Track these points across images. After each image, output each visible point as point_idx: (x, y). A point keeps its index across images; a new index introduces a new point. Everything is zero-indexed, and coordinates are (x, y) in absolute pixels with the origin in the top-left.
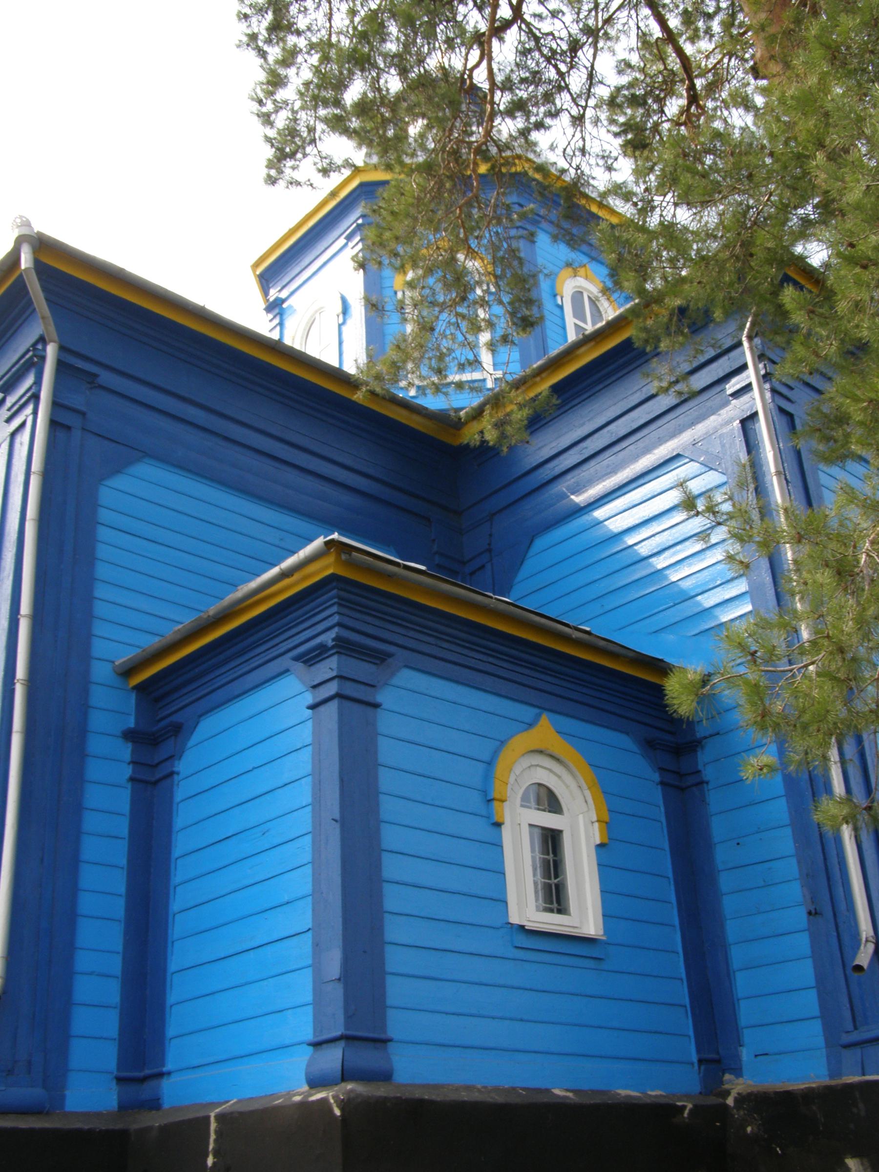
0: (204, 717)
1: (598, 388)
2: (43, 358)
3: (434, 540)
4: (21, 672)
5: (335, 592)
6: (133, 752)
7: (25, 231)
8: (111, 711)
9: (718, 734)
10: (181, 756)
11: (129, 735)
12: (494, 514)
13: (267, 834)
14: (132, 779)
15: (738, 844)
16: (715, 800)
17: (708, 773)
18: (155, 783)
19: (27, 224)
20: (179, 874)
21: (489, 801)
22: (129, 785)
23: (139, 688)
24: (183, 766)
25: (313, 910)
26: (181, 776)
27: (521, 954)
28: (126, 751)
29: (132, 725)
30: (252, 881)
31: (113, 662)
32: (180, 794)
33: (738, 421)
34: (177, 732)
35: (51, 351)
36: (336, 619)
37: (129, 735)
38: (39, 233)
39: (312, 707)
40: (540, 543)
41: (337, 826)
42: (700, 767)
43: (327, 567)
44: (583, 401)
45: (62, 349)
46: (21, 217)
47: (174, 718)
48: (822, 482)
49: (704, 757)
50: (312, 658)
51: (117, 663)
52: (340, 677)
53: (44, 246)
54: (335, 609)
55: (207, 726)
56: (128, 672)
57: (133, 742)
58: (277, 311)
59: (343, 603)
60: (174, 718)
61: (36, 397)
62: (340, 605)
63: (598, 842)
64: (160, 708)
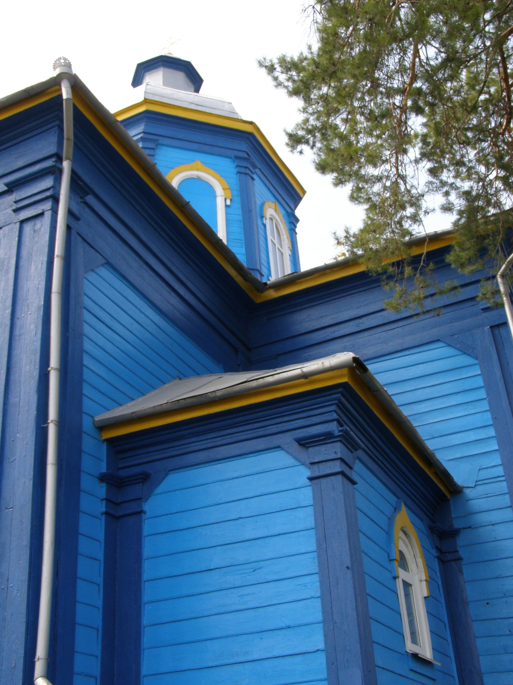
0: (171, 472)
1: (373, 286)
2: (60, 171)
3: (239, 365)
5: (339, 395)
6: (107, 490)
8: (95, 460)
9: (470, 527)
10: (147, 500)
11: (102, 478)
12: (279, 355)
13: (257, 571)
14: (106, 513)
15: (488, 604)
16: (468, 572)
17: (462, 553)
18: (118, 518)
19: (69, 65)
20: (148, 592)
21: (391, 560)
22: (103, 518)
23: (110, 441)
24: (148, 507)
25: (325, 636)
26: (147, 515)
27: (412, 675)
28: (102, 490)
29: (104, 470)
30: (244, 607)
31: (93, 417)
32: (147, 528)
33: (489, 327)
34: (146, 480)
35: (66, 165)
36: (335, 416)
37: (102, 478)
38: (75, 75)
39: (311, 479)
41: (349, 575)
42: (458, 549)
43: (342, 376)
44: (360, 292)
46: (65, 59)
47: (146, 468)
48: (85, 362)
49: (461, 540)
50: (304, 443)
51: (97, 419)
52: (342, 460)
53: (78, 88)
54: (334, 408)
55: (174, 480)
56: (102, 427)
57: (107, 483)
59: (340, 405)
60: (146, 468)
61: (56, 199)
62: (338, 406)
63: (426, 594)
64: (121, 459)
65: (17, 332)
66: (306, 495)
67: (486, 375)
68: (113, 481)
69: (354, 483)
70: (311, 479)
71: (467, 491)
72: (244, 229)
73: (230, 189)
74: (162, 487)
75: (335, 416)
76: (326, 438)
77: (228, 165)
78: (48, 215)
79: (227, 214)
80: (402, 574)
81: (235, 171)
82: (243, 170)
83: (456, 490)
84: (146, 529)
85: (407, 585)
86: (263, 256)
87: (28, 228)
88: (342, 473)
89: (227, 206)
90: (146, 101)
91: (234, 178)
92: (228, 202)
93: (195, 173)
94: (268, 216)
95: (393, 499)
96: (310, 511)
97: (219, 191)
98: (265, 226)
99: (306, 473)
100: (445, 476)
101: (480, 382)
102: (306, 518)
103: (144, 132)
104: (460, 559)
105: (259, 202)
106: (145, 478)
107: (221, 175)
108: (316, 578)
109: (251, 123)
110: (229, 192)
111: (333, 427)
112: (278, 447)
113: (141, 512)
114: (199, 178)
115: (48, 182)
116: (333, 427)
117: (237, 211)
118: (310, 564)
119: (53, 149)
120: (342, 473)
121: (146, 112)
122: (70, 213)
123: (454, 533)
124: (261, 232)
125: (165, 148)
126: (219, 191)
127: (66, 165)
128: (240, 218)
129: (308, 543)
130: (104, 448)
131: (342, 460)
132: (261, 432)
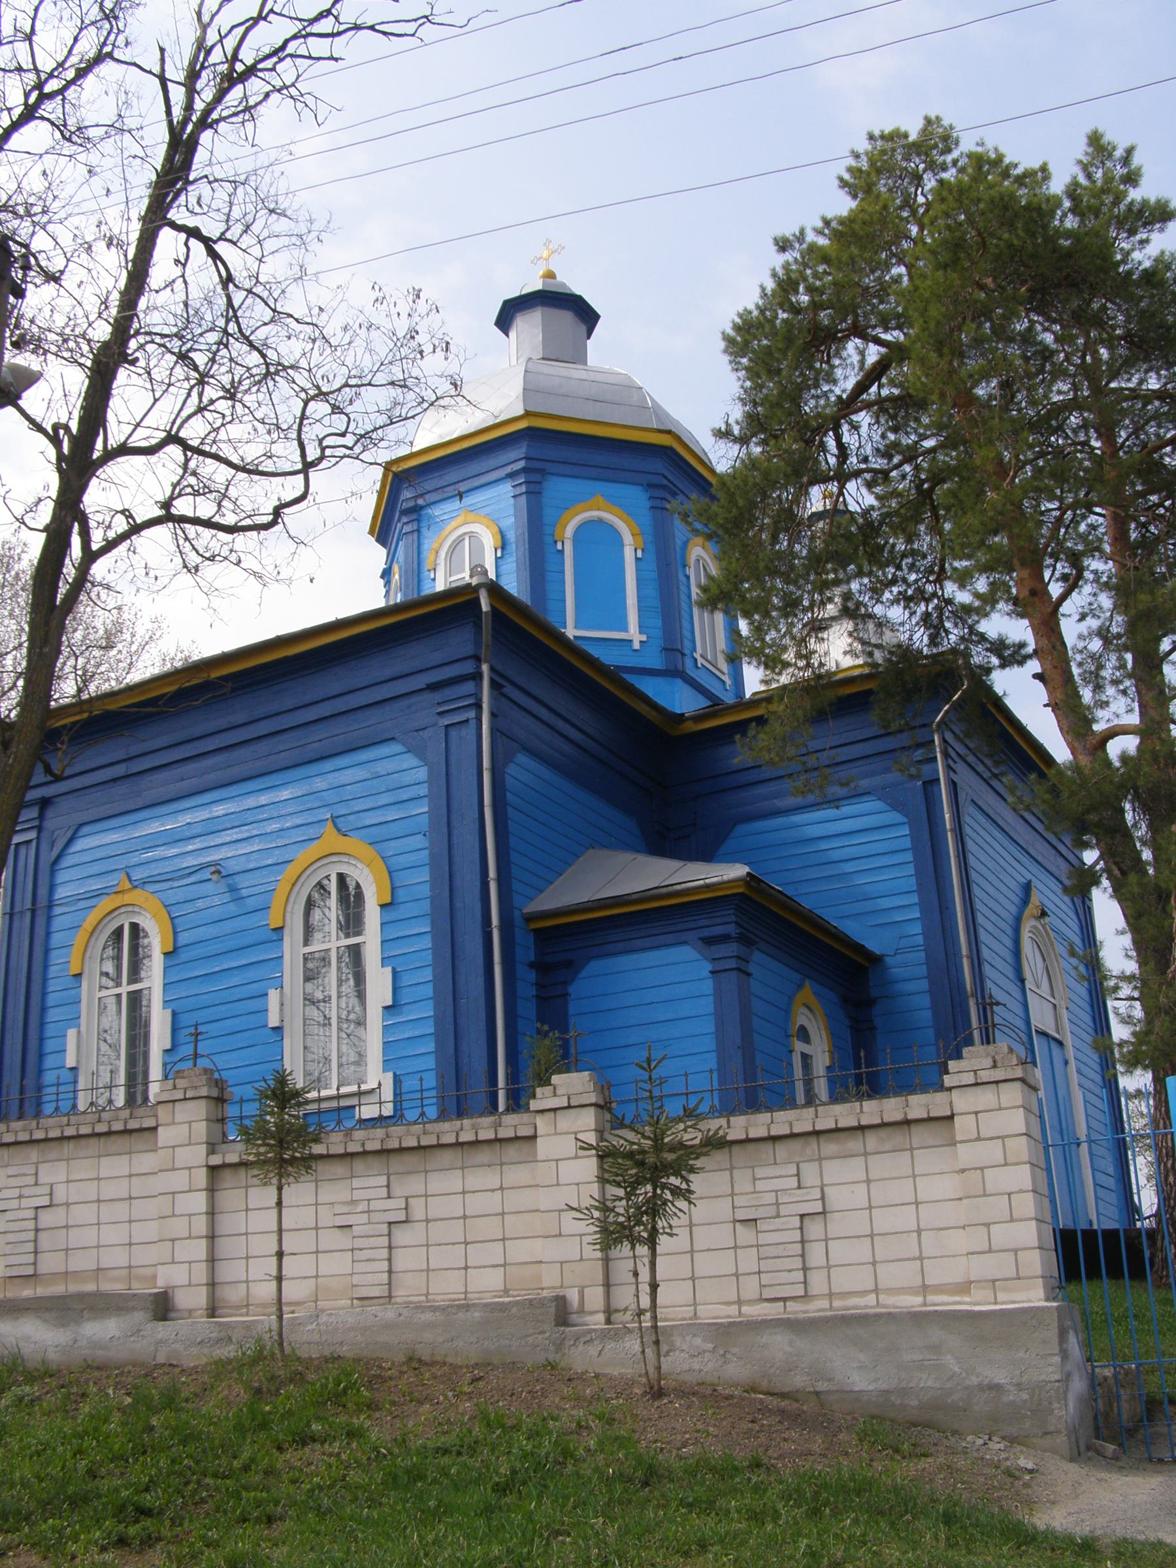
4: (495, 921)
7: (482, 580)
8: (526, 951)
11: (532, 965)
23: (536, 931)
24: (572, 989)
28: (532, 976)
34: (571, 967)
35: (485, 668)
36: (733, 918)
37: (532, 965)
39: (712, 972)
40: (741, 829)
45: (492, 669)
50: (709, 941)
51: (526, 910)
52: (738, 957)
55: (595, 967)
58: (414, 516)
61: (478, 706)
65: (455, 840)
66: (708, 986)
67: (914, 836)
68: (541, 967)
69: (749, 975)
70: (712, 972)
71: (887, 959)
72: (661, 595)
73: (642, 534)
74: (584, 973)
75: (733, 918)
76: (724, 939)
77: (637, 496)
78: (473, 723)
79: (637, 570)
80: (799, 1046)
81: (648, 504)
82: (658, 503)
83: (876, 960)
84: (572, 1010)
85: (805, 1057)
86: (686, 624)
87: (453, 733)
88: (738, 969)
89: (637, 559)
90: (528, 414)
91: (646, 516)
92: (639, 554)
93: (595, 514)
94: (692, 560)
95: (796, 976)
96: (711, 999)
97: (628, 538)
98: (688, 577)
99: (708, 967)
100: (860, 949)
101: (907, 842)
102: (707, 1005)
103: (526, 458)
104: (874, 1028)
105: (679, 543)
106: (569, 964)
107: (629, 514)
108: (714, 1054)
109: (669, 432)
110: (640, 539)
111: (731, 929)
112: (685, 943)
113: (566, 995)
114: (600, 521)
115: (469, 687)
116: (731, 929)
117: (651, 566)
118: (709, 1043)
119: (469, 650)
120: (738, 969)
121: (529, 429)
122: (493, 715)
123: (870, 1003)
124: (683, 588)
125: (555, 478)
126: (628, 538)
127: (485, 668)
128: (655, 575)
129: (709, 1026)
130: (531, 938)
131: (738, 957)
132: (671, 928)
